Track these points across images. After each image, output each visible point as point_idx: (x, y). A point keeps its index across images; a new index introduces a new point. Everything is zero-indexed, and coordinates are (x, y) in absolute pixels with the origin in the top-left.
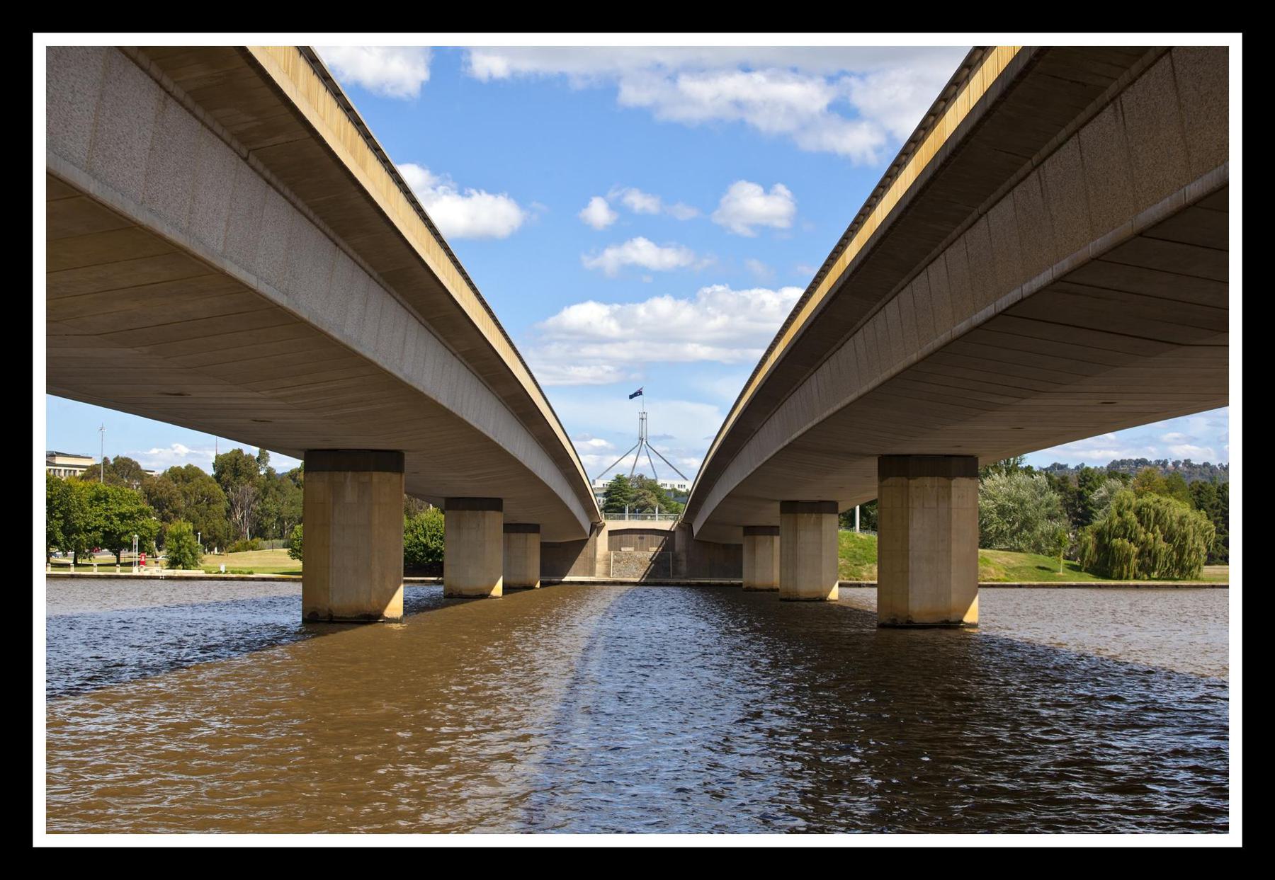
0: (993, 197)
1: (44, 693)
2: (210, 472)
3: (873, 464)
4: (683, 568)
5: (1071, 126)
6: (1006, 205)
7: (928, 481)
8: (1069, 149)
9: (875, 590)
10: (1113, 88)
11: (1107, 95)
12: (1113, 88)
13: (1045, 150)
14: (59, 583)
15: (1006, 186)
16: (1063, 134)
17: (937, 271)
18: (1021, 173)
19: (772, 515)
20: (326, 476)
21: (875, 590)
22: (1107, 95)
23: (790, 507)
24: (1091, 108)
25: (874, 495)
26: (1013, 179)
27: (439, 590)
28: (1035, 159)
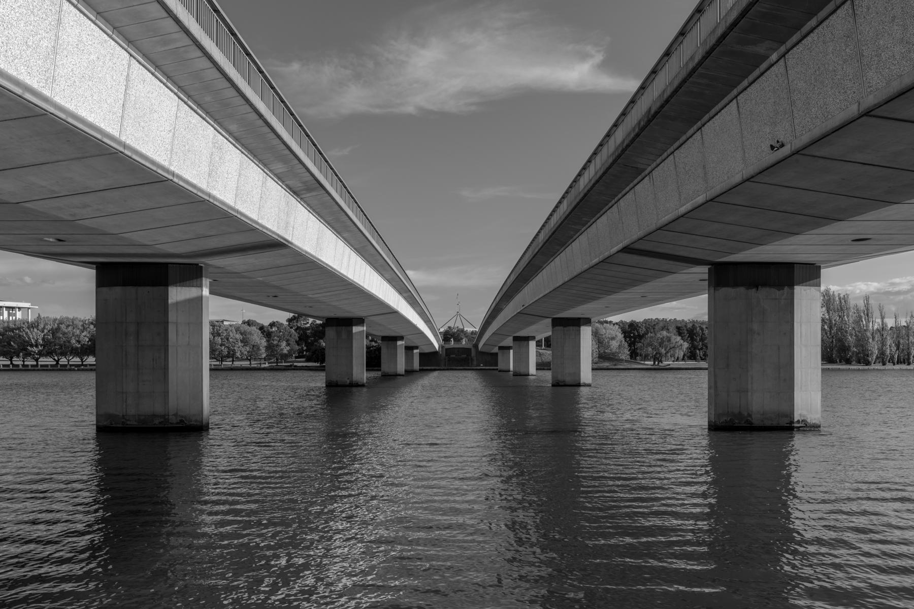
0: (598, 215)
1: (590, 367)
2: (286, 323)
3: (550, 320)
4: (475, 363)
5: (631, 185)
6: (604, 218)
7: (571, 328)
8: (630, 196)
9: (92, 376)
10: (649, 169)
11: (647, 172)
12: (649, 169)
13: (620, 196)
14: (600, 373)
15: (604, 210)
16: (628, 189)
17: (575, 245)
18: (610, 204)
19: (509, 342)
20: (334, 328)
21: (92, 376)
22: (647, 172)
23: (516, 339)
24: (640, 178)
25: (550, 333)
26: (607, 207)
27: (380, 373)
28: (616, 199)
